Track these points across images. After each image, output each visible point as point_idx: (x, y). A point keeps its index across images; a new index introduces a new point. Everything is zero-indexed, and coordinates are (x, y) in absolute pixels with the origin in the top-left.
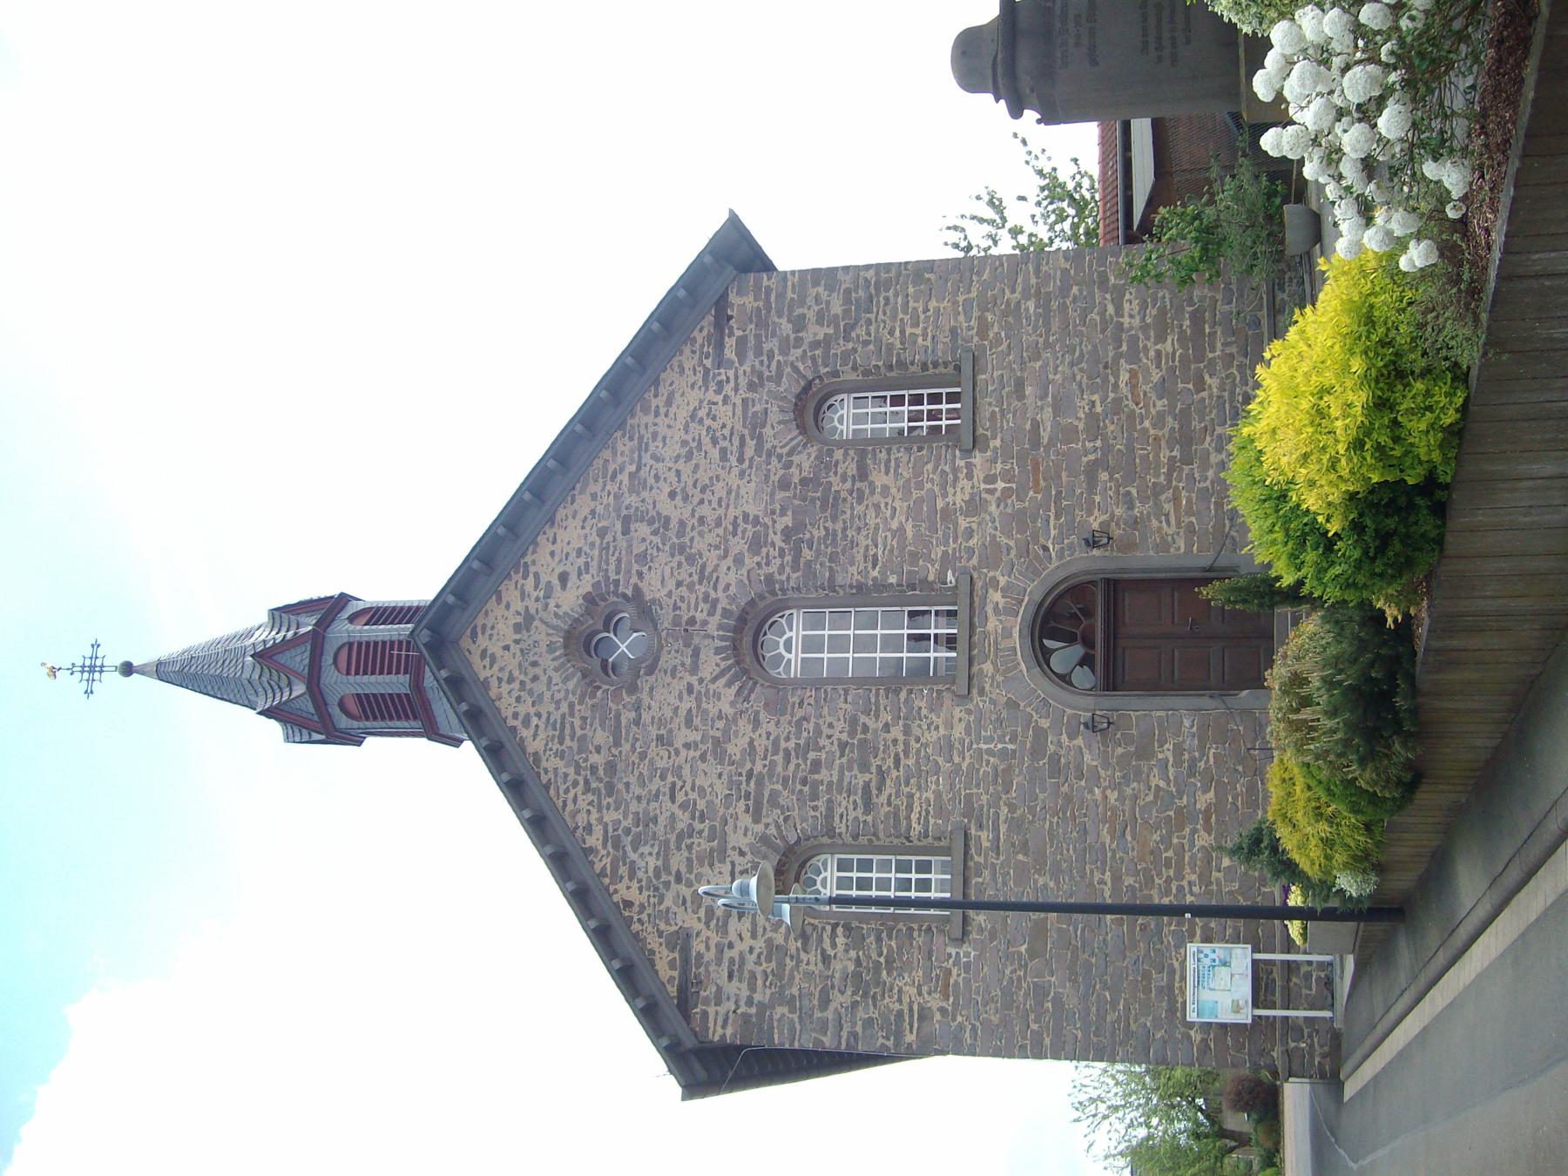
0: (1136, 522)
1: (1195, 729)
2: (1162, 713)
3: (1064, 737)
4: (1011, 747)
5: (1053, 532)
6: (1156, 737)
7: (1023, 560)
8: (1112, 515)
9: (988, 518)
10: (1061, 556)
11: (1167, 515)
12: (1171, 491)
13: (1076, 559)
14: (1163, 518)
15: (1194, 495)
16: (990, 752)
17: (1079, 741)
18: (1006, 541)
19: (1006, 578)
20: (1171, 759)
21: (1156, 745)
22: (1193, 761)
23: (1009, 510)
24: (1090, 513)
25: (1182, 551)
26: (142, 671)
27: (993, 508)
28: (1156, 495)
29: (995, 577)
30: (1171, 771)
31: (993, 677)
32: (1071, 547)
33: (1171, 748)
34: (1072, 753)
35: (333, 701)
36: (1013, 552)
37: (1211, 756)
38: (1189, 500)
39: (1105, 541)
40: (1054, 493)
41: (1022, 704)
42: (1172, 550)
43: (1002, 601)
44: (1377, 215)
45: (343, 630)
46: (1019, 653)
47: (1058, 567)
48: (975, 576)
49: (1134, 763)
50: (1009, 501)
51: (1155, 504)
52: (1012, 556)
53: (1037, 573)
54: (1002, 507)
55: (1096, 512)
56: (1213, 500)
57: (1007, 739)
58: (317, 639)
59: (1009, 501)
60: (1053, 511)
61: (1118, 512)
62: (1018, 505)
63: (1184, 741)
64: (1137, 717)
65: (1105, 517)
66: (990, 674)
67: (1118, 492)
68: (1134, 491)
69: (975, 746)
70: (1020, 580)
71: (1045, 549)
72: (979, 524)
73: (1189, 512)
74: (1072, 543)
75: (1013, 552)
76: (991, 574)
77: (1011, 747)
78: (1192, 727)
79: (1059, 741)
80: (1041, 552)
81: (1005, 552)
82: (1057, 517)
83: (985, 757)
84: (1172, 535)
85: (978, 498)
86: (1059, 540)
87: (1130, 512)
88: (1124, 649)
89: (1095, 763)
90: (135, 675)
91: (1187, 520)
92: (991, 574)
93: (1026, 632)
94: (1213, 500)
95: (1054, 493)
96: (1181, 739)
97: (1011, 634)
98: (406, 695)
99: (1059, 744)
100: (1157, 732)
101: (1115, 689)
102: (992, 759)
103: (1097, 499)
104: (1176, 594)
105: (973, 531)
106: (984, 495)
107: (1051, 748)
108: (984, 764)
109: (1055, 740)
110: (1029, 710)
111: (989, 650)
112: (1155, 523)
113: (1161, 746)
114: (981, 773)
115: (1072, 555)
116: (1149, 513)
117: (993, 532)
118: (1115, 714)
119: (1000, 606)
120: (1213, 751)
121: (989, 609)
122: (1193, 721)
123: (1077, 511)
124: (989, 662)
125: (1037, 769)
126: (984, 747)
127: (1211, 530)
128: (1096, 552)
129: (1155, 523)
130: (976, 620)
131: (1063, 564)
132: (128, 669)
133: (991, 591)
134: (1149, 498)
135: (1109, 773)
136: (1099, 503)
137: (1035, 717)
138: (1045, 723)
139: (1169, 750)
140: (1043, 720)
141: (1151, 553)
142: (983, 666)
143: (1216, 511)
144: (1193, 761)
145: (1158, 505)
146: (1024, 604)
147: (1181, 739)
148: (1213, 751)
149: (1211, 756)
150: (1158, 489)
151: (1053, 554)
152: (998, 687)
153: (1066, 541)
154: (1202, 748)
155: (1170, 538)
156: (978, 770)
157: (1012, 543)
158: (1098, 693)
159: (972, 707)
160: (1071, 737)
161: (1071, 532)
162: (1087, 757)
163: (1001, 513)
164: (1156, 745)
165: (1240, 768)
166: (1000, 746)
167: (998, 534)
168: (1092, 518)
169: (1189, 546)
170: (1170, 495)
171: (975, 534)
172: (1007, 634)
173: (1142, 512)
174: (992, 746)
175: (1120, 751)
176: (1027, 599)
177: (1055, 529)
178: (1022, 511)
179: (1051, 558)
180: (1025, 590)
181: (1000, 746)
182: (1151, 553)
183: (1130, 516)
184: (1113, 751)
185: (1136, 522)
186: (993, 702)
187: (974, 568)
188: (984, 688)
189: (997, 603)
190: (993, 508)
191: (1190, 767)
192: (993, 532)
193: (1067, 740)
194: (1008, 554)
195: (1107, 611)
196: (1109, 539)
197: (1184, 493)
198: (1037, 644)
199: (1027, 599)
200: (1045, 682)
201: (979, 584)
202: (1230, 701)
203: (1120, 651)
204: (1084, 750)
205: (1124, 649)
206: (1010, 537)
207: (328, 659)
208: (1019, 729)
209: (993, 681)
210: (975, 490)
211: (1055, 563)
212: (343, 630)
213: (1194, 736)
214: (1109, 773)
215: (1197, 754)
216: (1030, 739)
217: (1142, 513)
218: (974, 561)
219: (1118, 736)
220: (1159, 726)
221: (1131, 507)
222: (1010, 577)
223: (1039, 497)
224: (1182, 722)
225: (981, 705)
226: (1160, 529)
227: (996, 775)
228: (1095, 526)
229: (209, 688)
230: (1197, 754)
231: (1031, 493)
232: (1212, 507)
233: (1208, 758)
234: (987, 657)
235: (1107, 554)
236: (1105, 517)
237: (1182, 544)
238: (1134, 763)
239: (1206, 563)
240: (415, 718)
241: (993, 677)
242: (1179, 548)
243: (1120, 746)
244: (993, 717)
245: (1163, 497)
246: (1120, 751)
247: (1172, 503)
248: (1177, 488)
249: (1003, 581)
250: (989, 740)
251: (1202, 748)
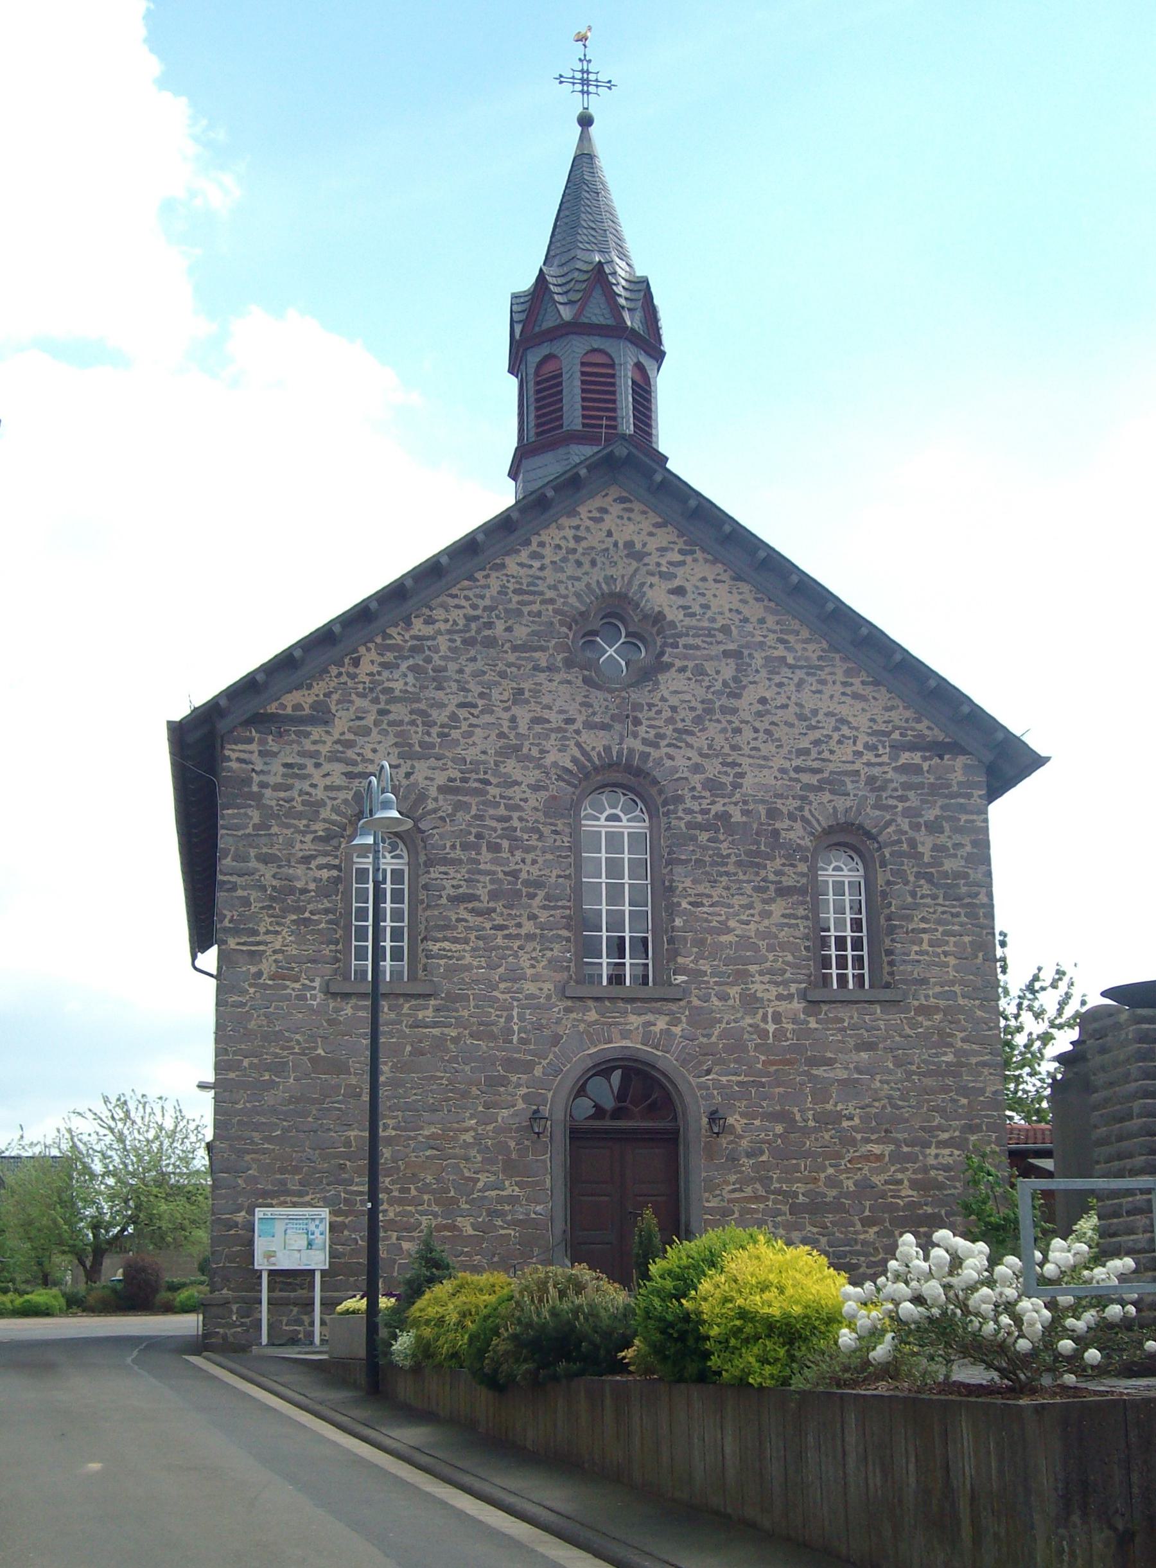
26: (584, 138)
35: (556, 348)
45: (627, 357)
58: (618, 331)
90: (580, 129)
98: (561, 426)
132: (585, 121)
212: (627, 357)
229: (559, 244)
240: (538, 434)
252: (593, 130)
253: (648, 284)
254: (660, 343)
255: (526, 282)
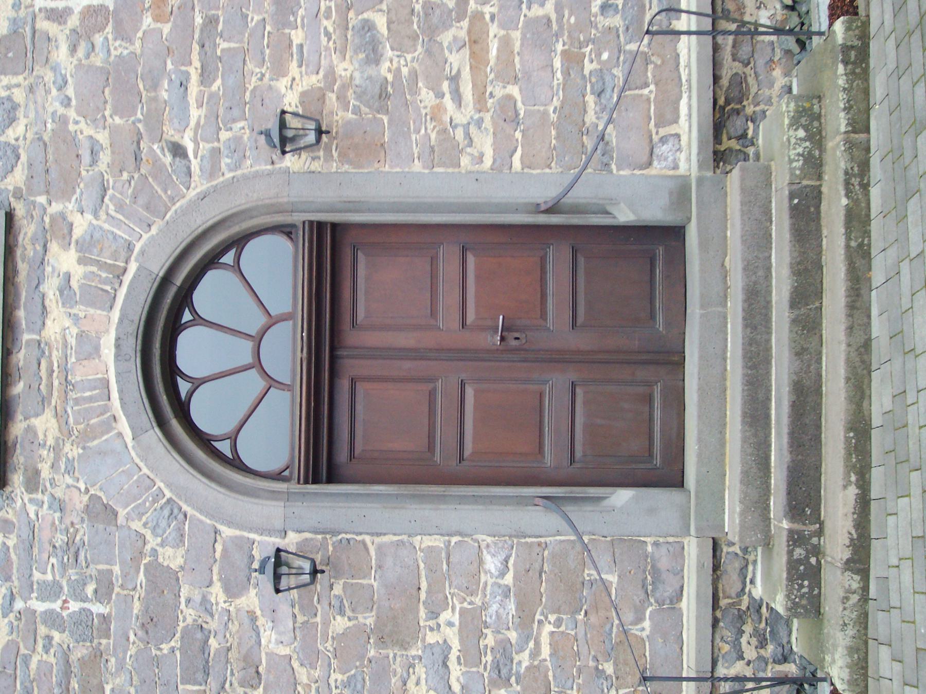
0: (383, 95)
1: (509, 579)
2: (437, 542)
3: (217, 592)
4: (97, 608)
5: (195, 114)
6: (423, 596)
7: (125, 175)
8: (331, 76)
9: (49, 76)
10: (213, 170)
11: (455, 79)
12: (465, 24)
13: (245, 177)
14: (445, 86)
15: (516, 35)
16: (52, 619)
17: (251, 600)
18: (89, 131)
19: (89, 217)
20: (455, 644)
21: (422, 613)
22: (505, 651)
23: (98, 60)
24: (280, 71)
25: (488, 162)
27: (61, 54)
28: (431, 32)
29: (63, 216)
30: (456, 671)
31: (57, 449)
32: (236, 147)
33: (456, 619)
34: (233, 627)
36: (105, 158)
37: (545, 639)
38: (505, 43)
39: (311, 137)
40: (199, 20)
41: (122, 513)
42: (465, 161)
43: (78, 272)
44: (46, 290)
46: (115, 395)
47: (203, 197)
48: (20, 210)
49: (372, 653)
50: (98, 39)
51: (428, 52)
52: (102, 166)
53: (155, 208)
54: (81, 53)
55: (294, 68)
56: (560, 47)
57: (90, 589)
59: (98, 39)
60: (197, 63)
61: (345, 68)
62: (119, 49)
63: (484, 607)
64: (380, 548)
65: (315, 80)
66: (50, 441)
67: (344, 26)
68: (381, 22)
69: (19, 605)
70: (118, 224)
71: (178, 151)
72: (31, 89)
73: (507, 75)
74: (238, 139)
75: (105, 158)
76: (55, 208)
77: (97, 608)
78: (502, 574)
79: (205, 600)
80: (168, 159)
81: (86, 158)
82: (206, 77)
83: (42, 630)
84: (467, 127)
85: (28, 29)
86: (215, 123)
87: (371, 71)
88: (353, 382)
89: (284, 651)
91: (499, 92)
92: (55, 208)
93: (132, 346)
94: (560, 47)
95: (199, 20)
96: (478, 601)
97: (97, 349)
99: (206, 606)
100: (424, 585)
101: (332, 479)
102: (57, 636)
103: (297, 36)
104: (471, 260)
105: (15, 107)
106: (43, 25)
107: (189, 615)
108: (40, 648)
109: (197, 598)
110: (136, 525)
111: (50, 386)
112: (427, 97)
113: (434, 615)
114: (33, 665)
115: (237, 166)
116: (414, 75)
117: (61, 110)
118: (331, 540)
119: (74, 284)
120: (548, 628)
121: (50, 288)
122: (506, 561)
123: (250, 66)
124: (48, 414)
125: (157, 661)
126: (40, 607)
127: (553, 117)
128: (290, 161)
129: (427, 97)
130: (21, 314)
131: (215, 189)
133: (54, 247)
134: (415, 38)
135: (316, 674)
136: (301, 46)
137: (153, 542)
138: (172, 558)
139: (450, 624)
140: (169, 551)
141: (417, 166)
142: (37, 422)
143: (566, 73)
144: (505, 651)
145: (433, 52)
146: (128, 278)
147: (478, 601)
148: (548, 628)
149: (545, 639)
150: (435, 20)
151: (195, 164)
152: (70, 471)
153: (224, 135)
154: (525, 620)
155: (459, 134)
156: (26, 660)
157: (102, 137)
158: (294, 487)
159: (11, 516)
160: (231, 592)
161: (236, 112)
162: (268, 637)
163: (79, 66)
164: (422, 613)
165: (609, 668)
166: (74, 606)
167: (72, 114)
168: (282, 84)
169: (504, 153)
170: (463, 34)
171: (20, 113)
172: (92, 351)
173: (398, 70)
174: (56, 605)
175: (340, 624)
176: (133, 267)
177: (200, 106)
178: (126, 65)
179: (190, 174)
180: (130, 247)
181: (74, 606)
182: (417, 166)
183: (370, 78)
184: (326, 623)
185: (383, 95)
186: (60, 506)
187: (18, 193)
188: (37, 472)
189: (68, 277)
190: (61, 54)
191: (497, 667)
192: (61, 110)
193: (222, 597)
194: (94, 162)
195: (434, 422)
196: (320, 132)
197: (493, 29)
198: (164, 399)
199: (133, 267)
200: (172, 463)
201: (27, 231)
202: (582, 515)
203: (344, 385)
204: (261, 621)
205: (353, 382)
206: (98, 121)
208: (117, 569)
209: (57, 459)
210: (22, 13)
211: (199, 185)
213: (506, 595)
214: (316, 674)
215: (513, 636)
216: (141, 592)
217: (398, 72)
218: (18, 177)
219: (338, 590)
220: (431, 570)
221: (374, 57)
222: (96, 215)
223: (166, 28)
224: (481, 562)
225: (32, 509)
226: (436, 113)
227: (67, 673)
228: (291, 101)
230: (513, 636)
231: (147, 21)
232: (557, 63)
233: (537, 644)
234: (44, 401)
235: (316, 166)
236: (314, 79)
237: (485, 144)
238: (372, 653)
239: (545, 193)
241: (57, 449)
242: (480, 158)
243: (342, 612)
244: (60, 539)
245: (446, 38)
246: (340, 624)
247: (466, 52)
248: (478, 17)
249: (81, 224)
250: (51, 591)
251: (525, 620)
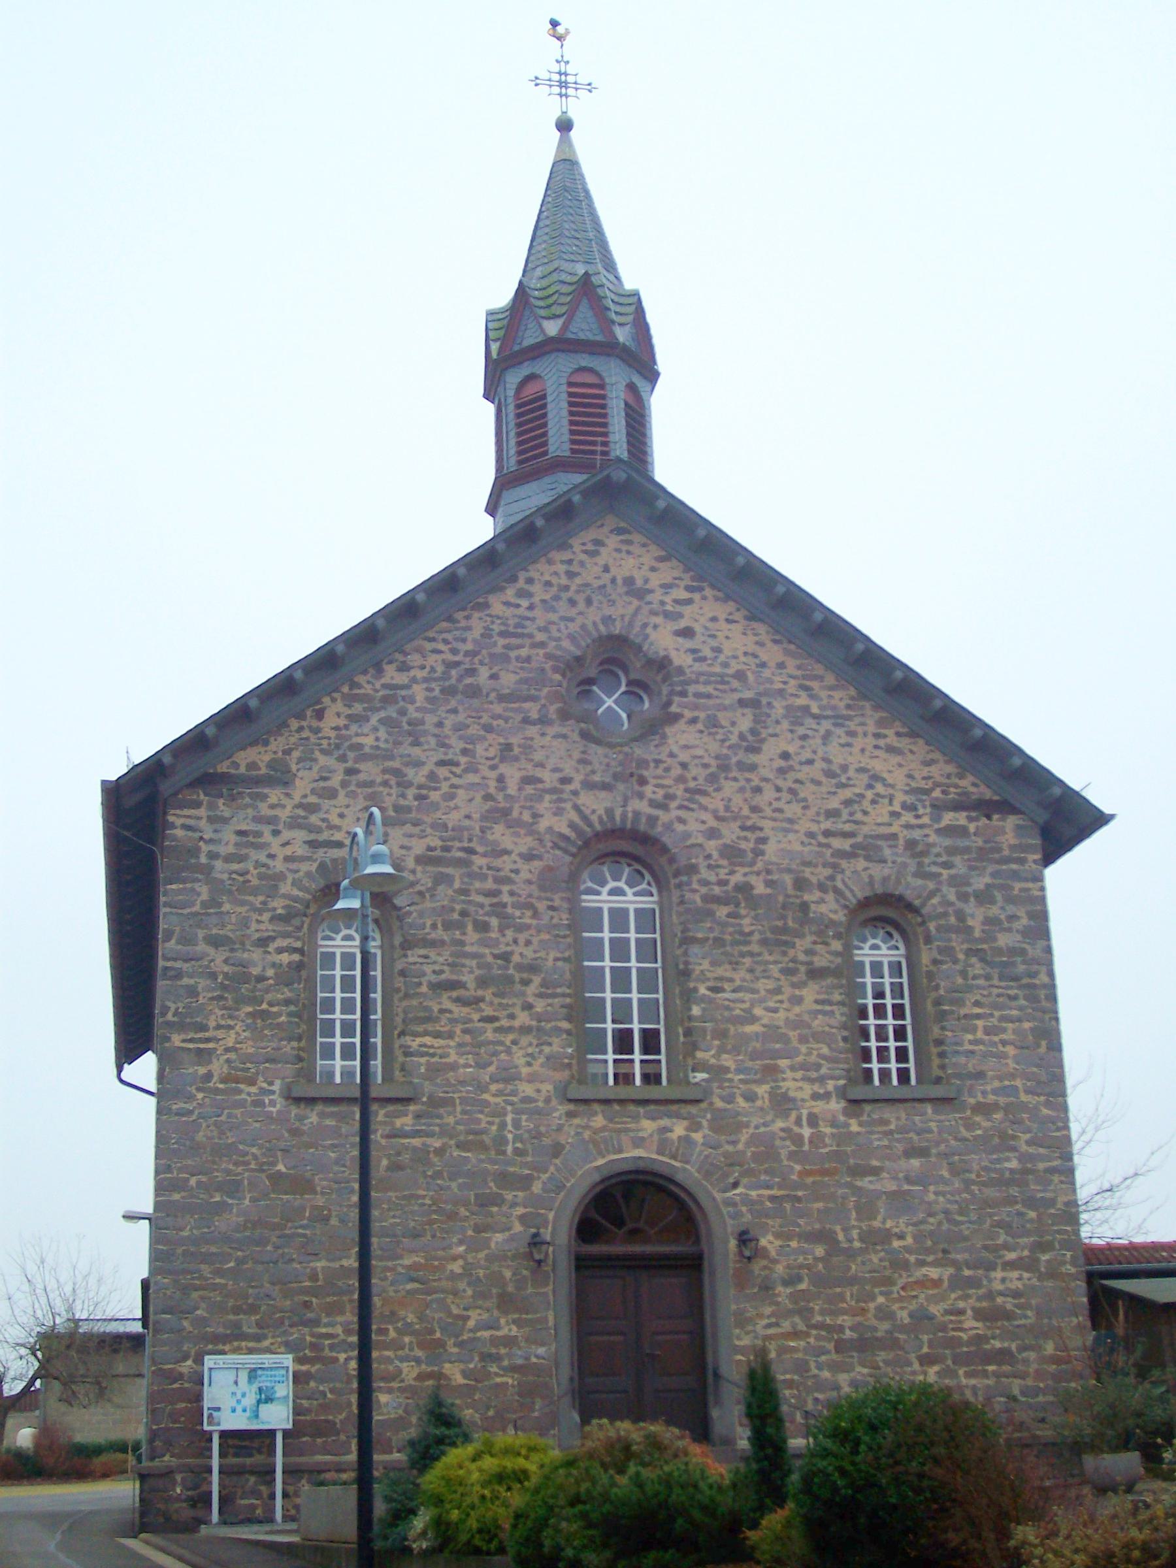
45: (616, 376)
58: (609, 348)
98: (546, 453)
132: (564, 126)
207: (585, 361)
212: (616, 376)
240: (520, 462)
252: (572, 133)
253: (639, 301)
254: (654, 362)
255: (503, 296)
